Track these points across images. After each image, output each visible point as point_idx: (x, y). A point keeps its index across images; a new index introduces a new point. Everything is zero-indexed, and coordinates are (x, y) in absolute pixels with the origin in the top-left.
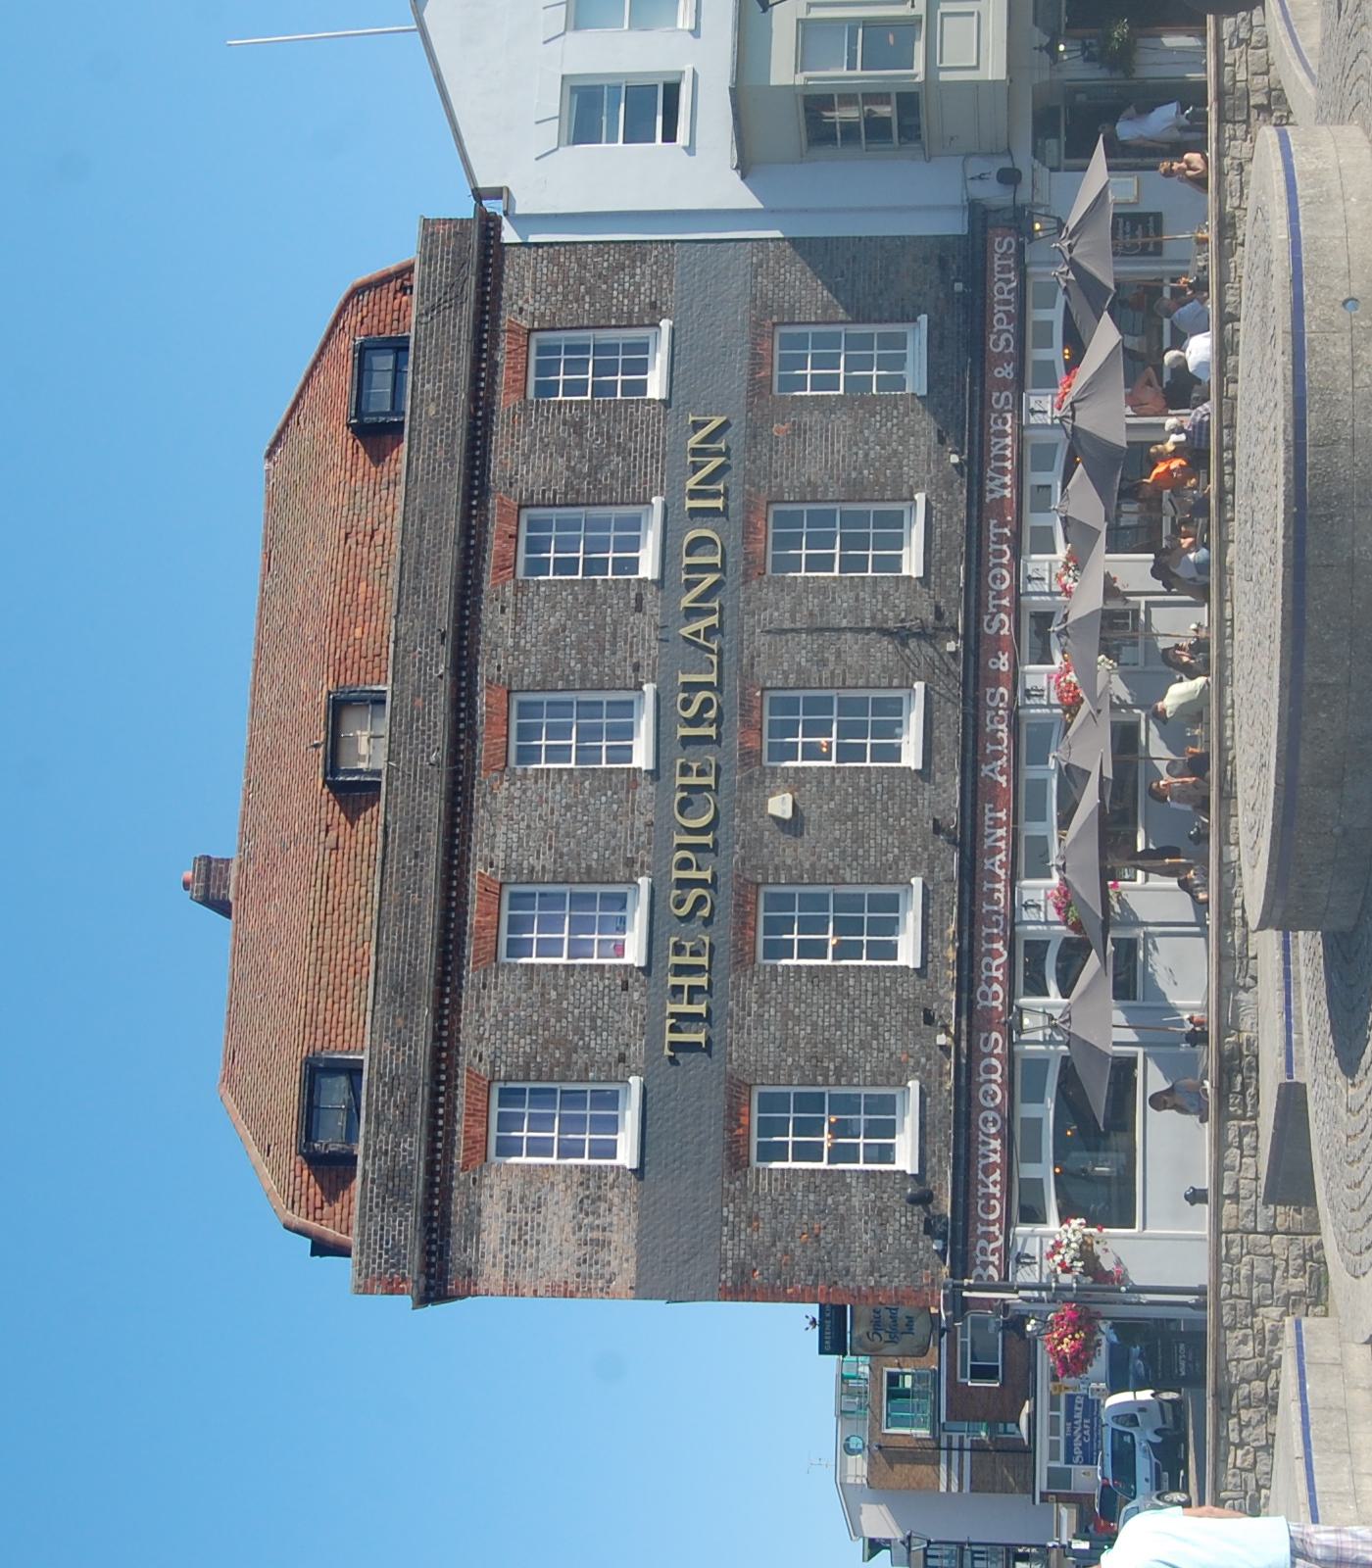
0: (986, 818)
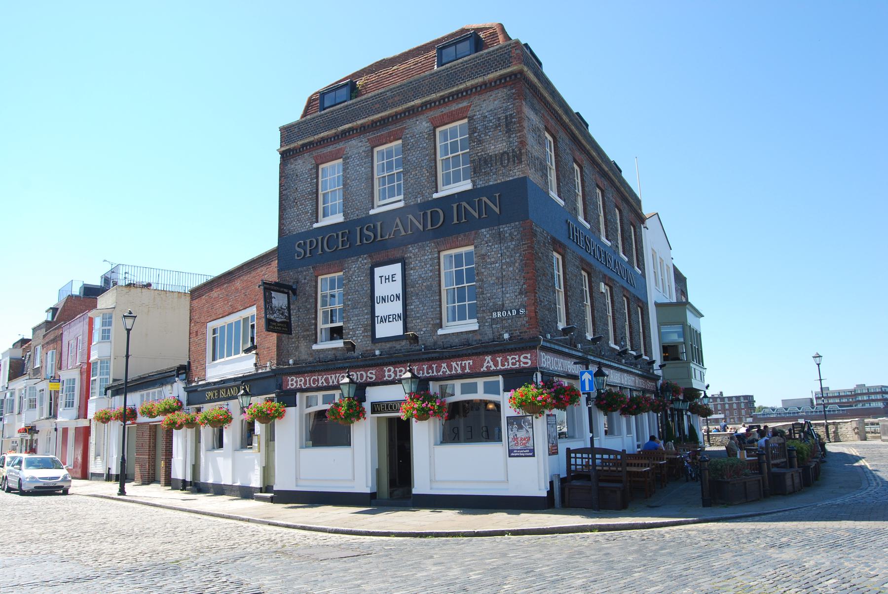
0: (465, 362)
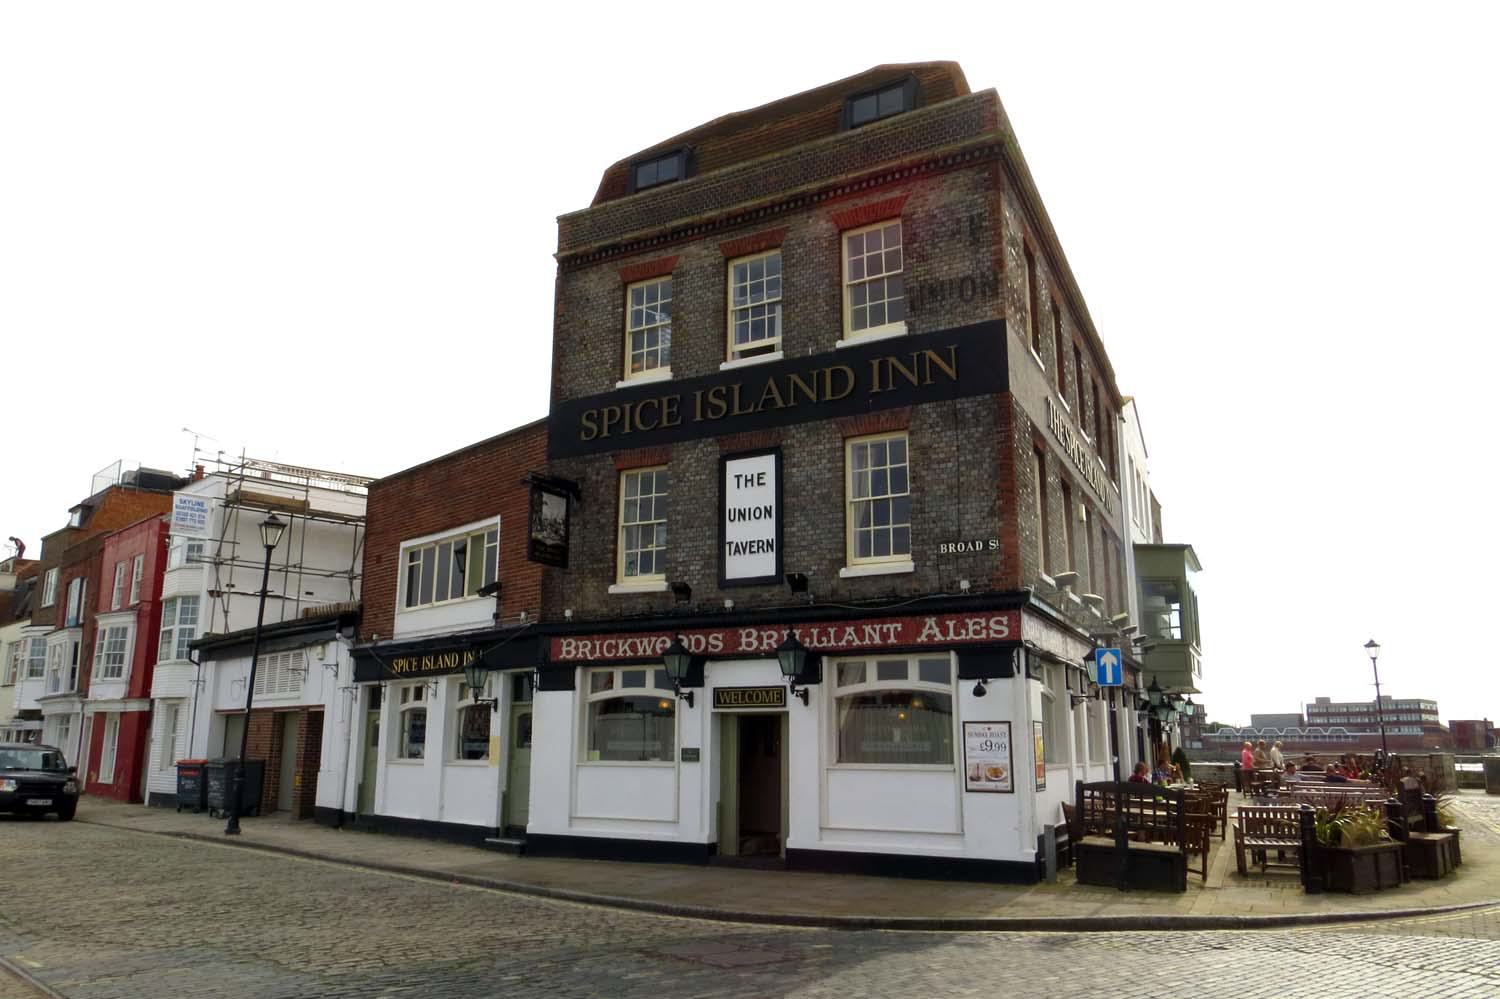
0: (888, 625)
